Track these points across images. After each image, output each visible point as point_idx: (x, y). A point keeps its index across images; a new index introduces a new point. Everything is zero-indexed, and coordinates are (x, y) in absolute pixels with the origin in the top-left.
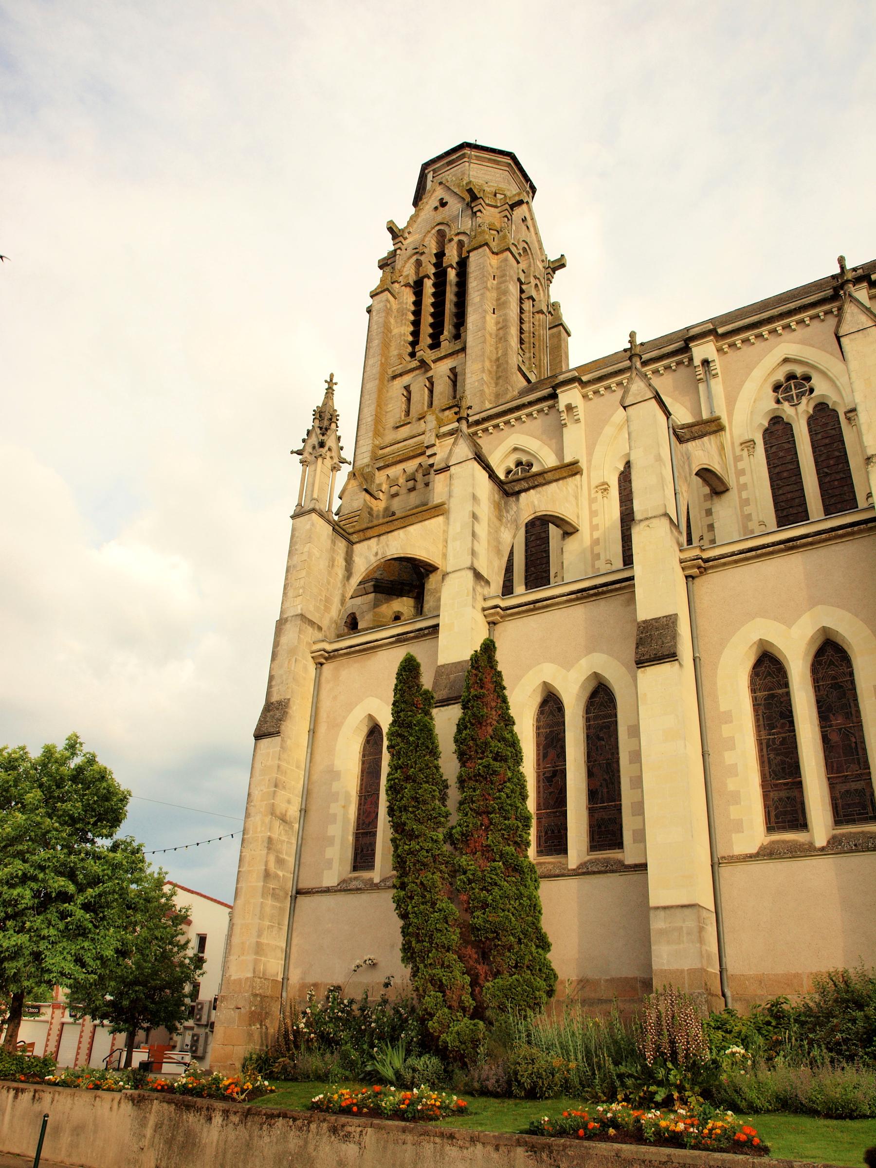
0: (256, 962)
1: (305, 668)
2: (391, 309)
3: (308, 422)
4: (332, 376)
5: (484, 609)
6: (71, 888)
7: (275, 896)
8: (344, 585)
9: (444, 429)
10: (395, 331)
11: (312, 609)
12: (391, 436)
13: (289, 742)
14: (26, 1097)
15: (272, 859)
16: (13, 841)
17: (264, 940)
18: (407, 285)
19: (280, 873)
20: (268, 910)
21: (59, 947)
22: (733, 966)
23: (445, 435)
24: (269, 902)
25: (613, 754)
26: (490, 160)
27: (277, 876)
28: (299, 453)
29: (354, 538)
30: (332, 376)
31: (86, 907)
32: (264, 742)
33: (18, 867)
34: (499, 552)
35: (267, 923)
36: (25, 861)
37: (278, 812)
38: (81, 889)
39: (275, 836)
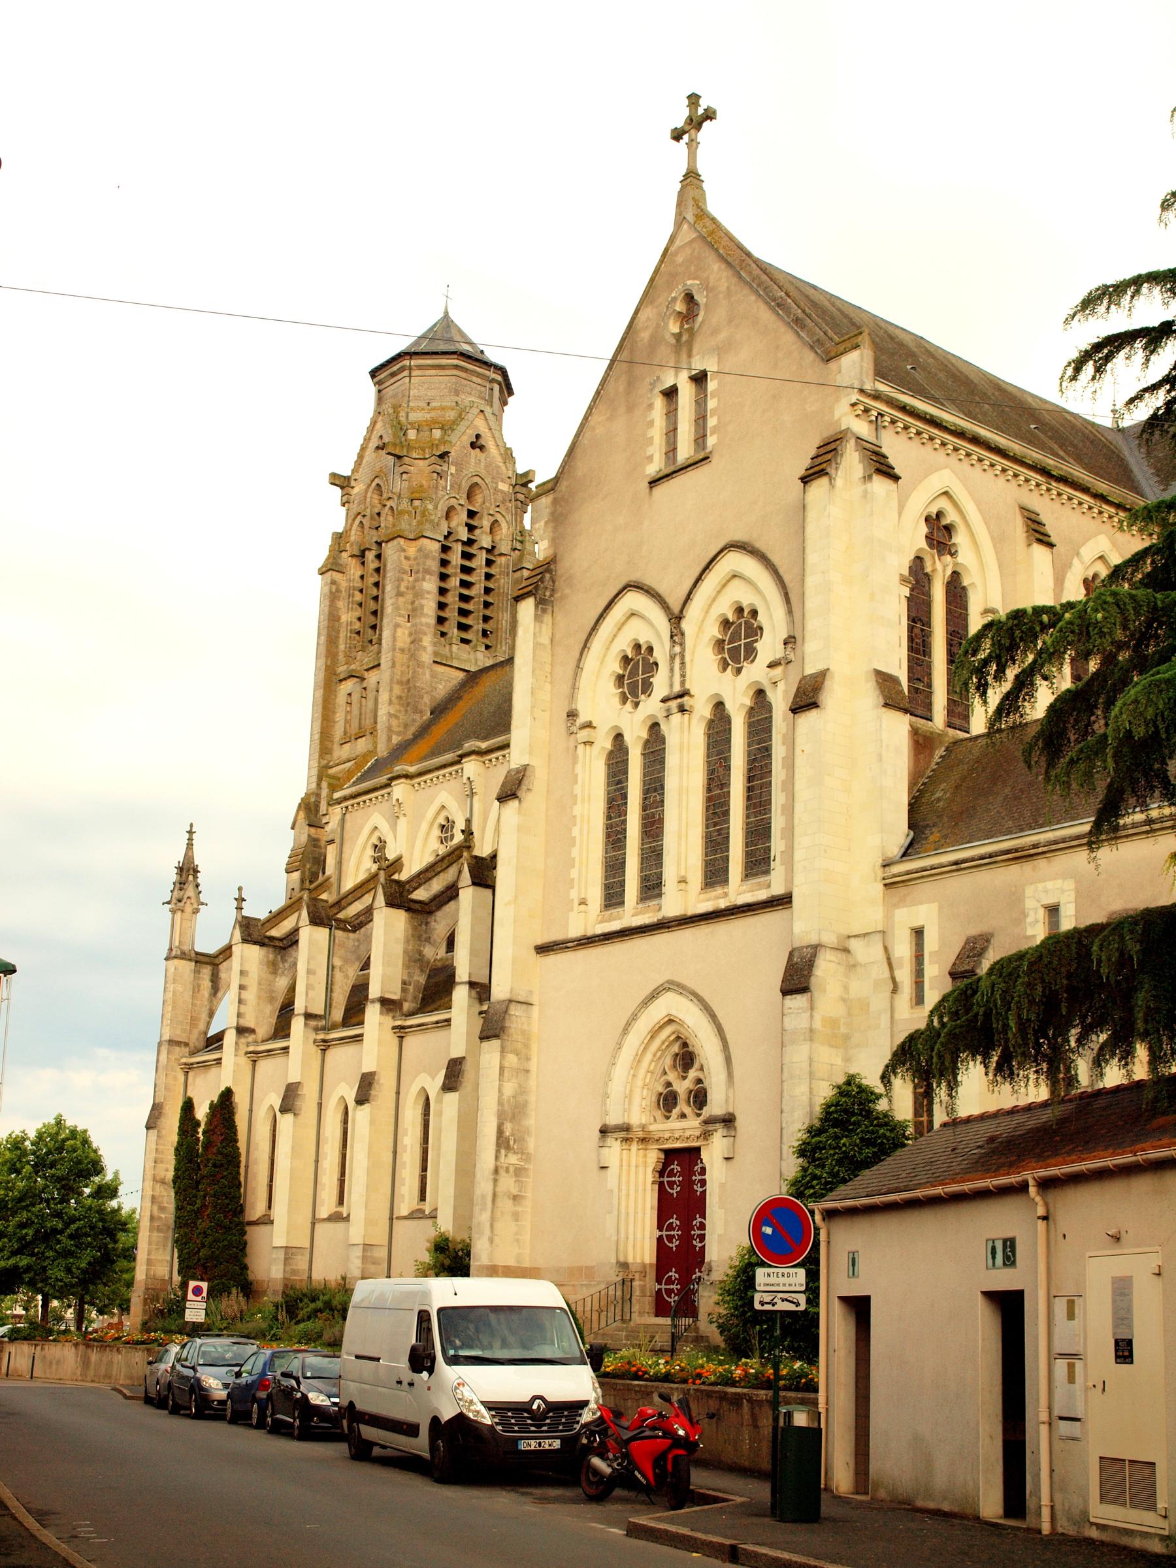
0: (147, 1270)
1: (175, 1078)
2: (338, 590)
3: (173, 876)
4: (191, 825)
5: (247, 1053)
7: (159, 1230)
9: (337, 795)
10: (344, 618)
13: (164, 1132)
14: (39, 1348)
15: (155, 1208)
19: (163, 1216)
24: (155, 1234)
25: (1136, 923)
27: (160, 1218)
28: (168, 903)
29: (217, 961)
30: (191, 825)
31: (71, 1237)
32: (151, 1131)
34: (272, 1000)
39: (157, 1194)
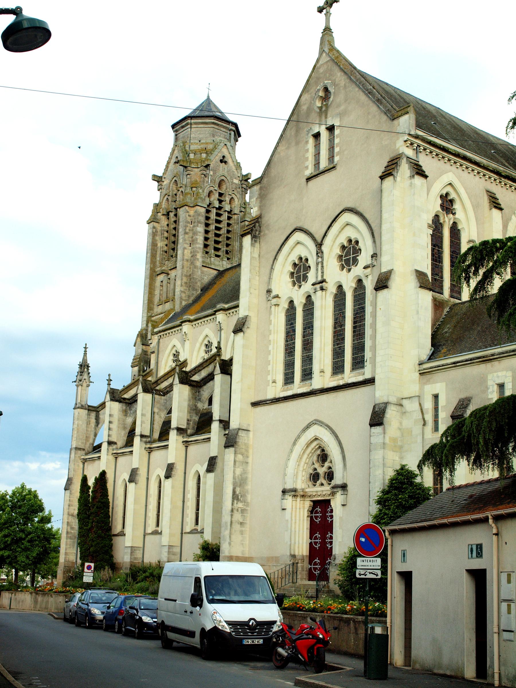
1: (78, 466)
2: (156, 231)
4: (86, 345)
6: (24, 536)
8: (95, 429)
11: (80, 444)
12: (158, 309)
13: (73, 491)
15: (69, 528)
16: (5, 524)
17: (68, 551)
18: (163, 215)
20: (68, 543)
21: (21, 554)
22: (145, 561)
23: (157, 333)
24: (69, 540)
26: (203, 123)
27: (71, 533)
28: (75, 382)
31: (29, 541)
33: (6, 532)
34: (125, 428)
35: (68, 546)
36: (8, 529)
37: (70, 514)
38: (27, 536)
